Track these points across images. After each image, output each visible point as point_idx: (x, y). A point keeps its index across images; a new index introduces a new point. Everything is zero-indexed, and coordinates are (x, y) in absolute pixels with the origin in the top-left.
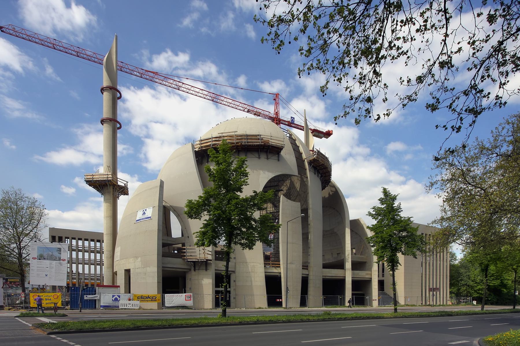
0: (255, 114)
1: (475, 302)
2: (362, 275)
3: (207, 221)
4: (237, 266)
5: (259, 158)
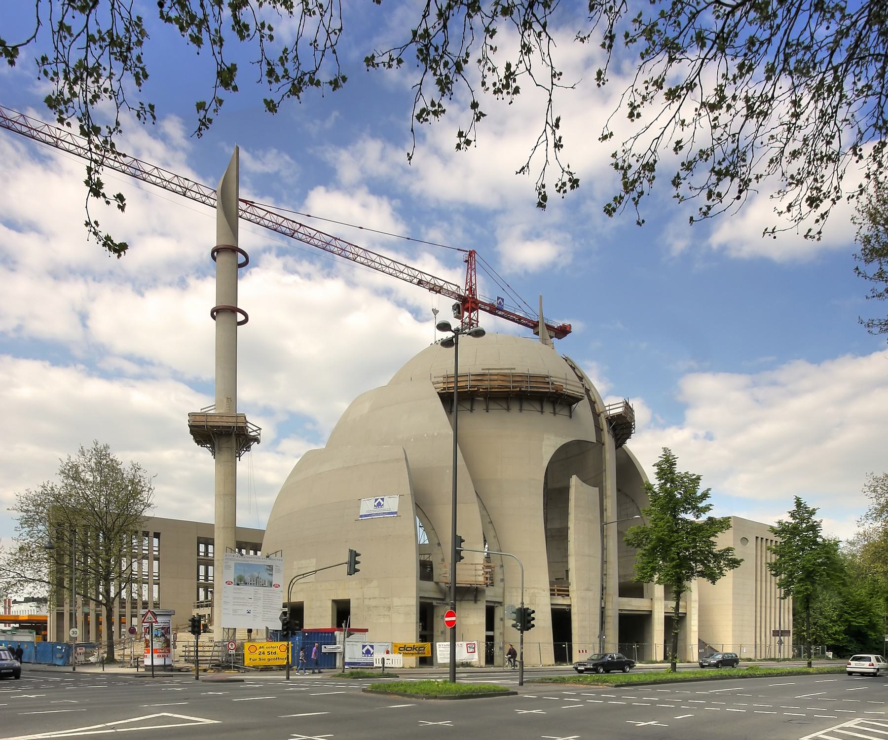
0: (430, 289)
1: (830, 654)
2: (635, 604)
3: (787, 594)
4: (507, 593)
5: (542, 412)
